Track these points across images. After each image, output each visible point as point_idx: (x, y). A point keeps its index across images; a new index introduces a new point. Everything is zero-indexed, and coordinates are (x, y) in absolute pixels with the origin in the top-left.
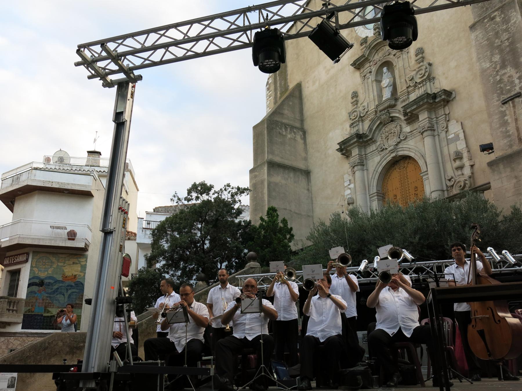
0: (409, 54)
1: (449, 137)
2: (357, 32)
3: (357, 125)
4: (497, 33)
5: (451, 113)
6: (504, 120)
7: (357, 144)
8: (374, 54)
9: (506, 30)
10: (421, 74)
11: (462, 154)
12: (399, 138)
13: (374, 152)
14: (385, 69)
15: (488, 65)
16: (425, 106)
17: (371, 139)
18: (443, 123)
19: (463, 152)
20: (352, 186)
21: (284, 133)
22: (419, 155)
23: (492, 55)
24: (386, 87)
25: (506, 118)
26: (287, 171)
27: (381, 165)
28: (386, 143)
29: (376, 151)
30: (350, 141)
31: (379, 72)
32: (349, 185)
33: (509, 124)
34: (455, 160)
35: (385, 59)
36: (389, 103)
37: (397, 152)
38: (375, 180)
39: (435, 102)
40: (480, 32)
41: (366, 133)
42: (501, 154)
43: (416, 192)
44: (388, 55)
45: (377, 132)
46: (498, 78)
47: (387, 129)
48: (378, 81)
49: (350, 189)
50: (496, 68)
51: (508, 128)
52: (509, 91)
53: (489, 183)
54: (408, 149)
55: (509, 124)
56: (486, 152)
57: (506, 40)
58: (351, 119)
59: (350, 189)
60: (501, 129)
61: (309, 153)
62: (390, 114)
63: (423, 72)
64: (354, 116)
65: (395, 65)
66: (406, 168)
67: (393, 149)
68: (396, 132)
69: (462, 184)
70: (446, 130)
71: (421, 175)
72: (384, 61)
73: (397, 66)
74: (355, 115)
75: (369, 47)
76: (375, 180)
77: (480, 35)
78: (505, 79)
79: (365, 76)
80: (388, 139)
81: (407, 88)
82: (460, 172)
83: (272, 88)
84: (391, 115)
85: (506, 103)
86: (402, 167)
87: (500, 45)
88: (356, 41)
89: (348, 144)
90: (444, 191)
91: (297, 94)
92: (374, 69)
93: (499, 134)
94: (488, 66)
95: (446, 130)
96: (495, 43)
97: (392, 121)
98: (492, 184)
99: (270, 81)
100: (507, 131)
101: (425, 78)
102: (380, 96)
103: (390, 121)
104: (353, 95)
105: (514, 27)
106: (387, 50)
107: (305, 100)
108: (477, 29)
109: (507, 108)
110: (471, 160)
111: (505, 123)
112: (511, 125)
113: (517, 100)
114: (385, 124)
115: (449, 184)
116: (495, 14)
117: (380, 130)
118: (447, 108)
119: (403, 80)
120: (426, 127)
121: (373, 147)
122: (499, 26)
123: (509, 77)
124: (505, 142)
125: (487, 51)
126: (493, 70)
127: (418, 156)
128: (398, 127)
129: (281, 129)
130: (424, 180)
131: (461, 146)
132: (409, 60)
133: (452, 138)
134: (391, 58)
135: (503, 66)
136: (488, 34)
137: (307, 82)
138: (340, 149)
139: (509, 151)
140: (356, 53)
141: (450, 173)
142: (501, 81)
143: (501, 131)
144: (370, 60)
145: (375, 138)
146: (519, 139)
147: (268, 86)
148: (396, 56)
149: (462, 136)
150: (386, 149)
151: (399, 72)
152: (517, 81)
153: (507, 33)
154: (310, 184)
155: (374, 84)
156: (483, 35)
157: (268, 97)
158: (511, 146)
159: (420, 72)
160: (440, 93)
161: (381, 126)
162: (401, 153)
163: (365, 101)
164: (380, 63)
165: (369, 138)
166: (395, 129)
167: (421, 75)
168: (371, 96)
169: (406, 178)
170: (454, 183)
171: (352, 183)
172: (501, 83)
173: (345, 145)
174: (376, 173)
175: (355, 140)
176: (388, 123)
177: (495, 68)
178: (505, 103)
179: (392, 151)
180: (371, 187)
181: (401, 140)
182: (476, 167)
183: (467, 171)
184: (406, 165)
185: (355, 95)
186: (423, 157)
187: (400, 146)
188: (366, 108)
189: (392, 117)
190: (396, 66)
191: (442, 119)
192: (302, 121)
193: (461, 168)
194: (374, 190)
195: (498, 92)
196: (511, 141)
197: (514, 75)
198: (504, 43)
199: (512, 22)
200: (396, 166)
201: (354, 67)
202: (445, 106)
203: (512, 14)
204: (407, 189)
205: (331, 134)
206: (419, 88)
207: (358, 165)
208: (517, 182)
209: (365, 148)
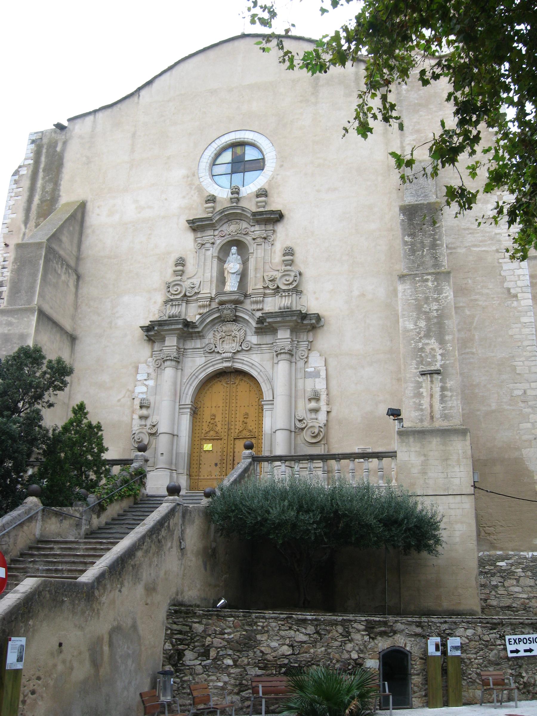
0: (273, 247)
1: (307, 370)
2: (201, 180)
3: (179, 305)
4: (427, 298)
5: (313, 343)
6: (419, 391)
7: (178, 332)
8: (223, 222)
9: (437, 300)
10: (288, 281)
11: (320, 395)
12: (241, 346)
13: (197, 350)
14: (234, 249)
15: (412, 326)
16: (291, 324)
17: (199, 332)
18: (304, 351)
19: (321, 393)
20: (151, 383)
21: (59, 272)
22: (265, 378)
23: (418, 318)
24: (234, 273)
25: (421, 390)
26: (55, 330)
27: (205, 370)
28: (219, 345)
29: (202, 350)
30: (172, 325)
31: (225, 250)
32: (145, 380)
33: (423, 397)
34: (310, 400)
35: (238, 236)
36: (237, 297)
37: (233, 362)
38: (192, 388)
39: (302, 323)
40: (409, 287)
41: (195, 323)
42: (410, 425)
43: (245, 420)
44: (245, 234)
45: (209, 327)
46: (420, 345)
47: (224, 328)
48: (222, 260)
49: (146, 386)
50: (419, 334)
51: (422, 402)
52: (429, 364)
53: (396, 452)
54: (250, 365)
55: (423, 397)
56: (392, 417)
57: (435, 310)
58: (169, 292)
59: (146, 386)
60: (414, 400)
61: (79, 311)
62: (236, 311)
63: (291, 279)
64: (176, 291)
65: (251, 251)
66: (237, 386)
67: (230, 358)
68: (238, 336)
69: (316, 431)
70: (306, 360)
71: (263, 403)
72: (236, 238)
73: (255, 254)
74: (178, 289)
75: (222, 213)
76: (192, 388)
77: (409, 291)
78: (428, 349)
79: (203, 244)
80: (223, 341)
81: (264, 288)
82: (313, 416)
83: (26, 183)
84: (237, 314)
85: (424, 374)
86: (232, 383)
87: (428, 312)
88: (198, 191)
89: (166, 328)
90: (291, 431)
91: (79, 216)
92: (219, 242)
93: (411, 404)
94: (412, 328)
95: (306, 360)
96: (423, 307)
97: (234, 321)
98: (398, 454)
99: (24, 171)
100: (421, 405)
101: (291, 287)
102: (222, 280)
103: (232, 320)
104: (179, 262)
105: (445, 301)
106: (243, 228)
107: (88, 231)
108: (406, 283)
109: (424, 380)
110: (328, 405)
111: (419, 395)
112: (425, 399)
113: (435, 376)
114: (223, 321)
115: (299, 425)
116: (429, 277)
117: (214, 325)
118: (311, 334)
119: (259, 275)
120: (286, 348)
121: (198, 343)
122: (430, 292)
123: (432, 349)
124: (417, 414)
125: (413, 311)
126: (416, 335)
127: (262, 378)
128: (242, 332)
129: (57, 263)
130: (264, 410)
131: (320, 385)
132: (272, 254)
133: (311, 372)
134: (247, 240)
135: (427, 336)
136: (417, 294)
137: (98, 207)
138: (147, 328)
139: (419, 426)
140: (194, 206)
141: (301, 413)
142: (422, 349)
143: (414, 402)
144: (215, 227)
145: (204, 332)
146: (430, 417)
147: (16, 177)
148: (256, 241)
149: (323, 374)
150: (218, 352)
151: (256, 261)
152: (439, 357)
153: (437, 304)
154: (73, 356)
155: (215, 261)
156: (411, 292)
157: (13, 194)
158: (421, 421)
159: (287, 278)
160: (311, 316)
161: (216, 321)
162: (238, 366)
163: (195, 277)
164: (230, 239)
165: (197, 330)
166: (237, 333)
167: (287, 281)
168: (208, 275)
169: (234, 398)
170: (306, 426)
171: (151, 379)
172: (423, 352)
173: (161, 328)
174: (195, 379)
175: (180, 326)
176: (228, 321)
177: (419, 333)
178: (423, 374)
179: (227, 360)
180: (185, 395)
181: (242, 349)
182: (333, 414)
183: (322, 417)
184: (237, 382)
185: (181, 262)
186: (270, 381)
187: (239, 356)
188: (197, 287)
189: (236, 316)
190: (253, 253)
191: (303, 345)
192: (78, 259)
193: (316, 411)
194: (188, 400)
195: (418, 359)
196: (422, 415)
197: (437, 350)
198: (432, 312)
199: (444, 295)
200: (222, 378)
201: (191, 225)
202: (309, 331)
203: (445, 287)
204: (233, 412)
205: (126, 299)
206: (282, 296)
207: (167, 360)
208: (425, 460)
209: (185, 340)
